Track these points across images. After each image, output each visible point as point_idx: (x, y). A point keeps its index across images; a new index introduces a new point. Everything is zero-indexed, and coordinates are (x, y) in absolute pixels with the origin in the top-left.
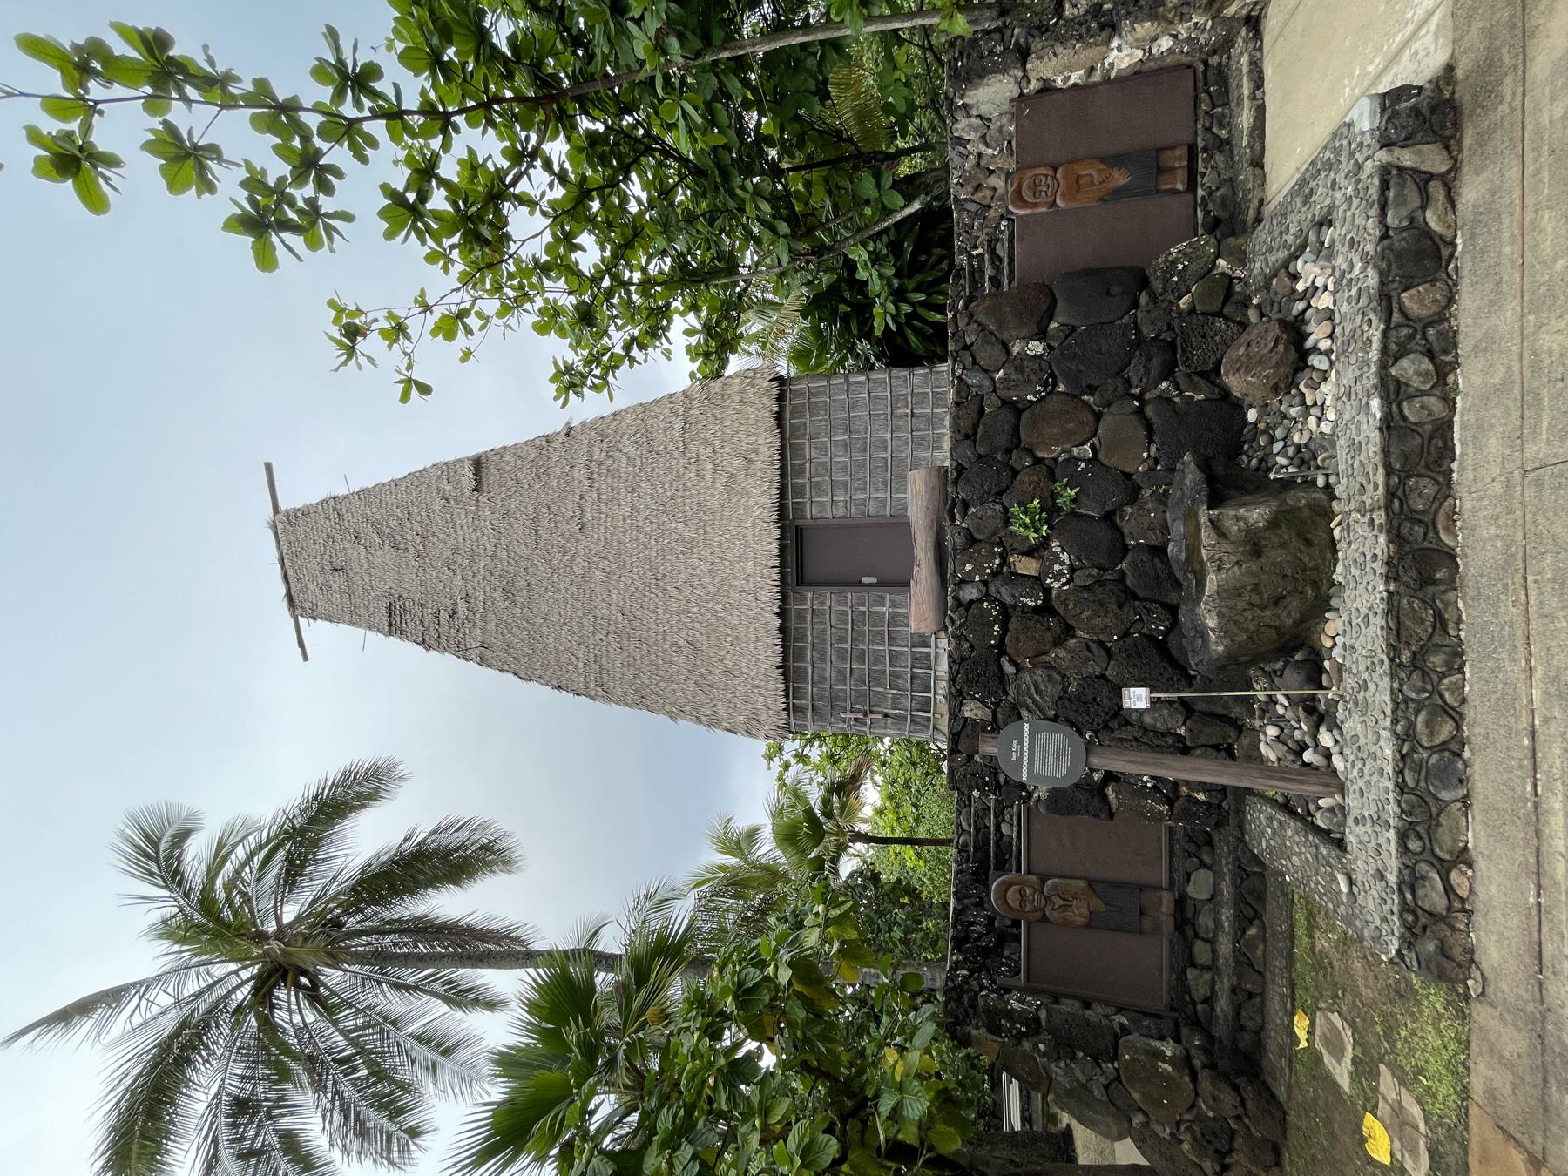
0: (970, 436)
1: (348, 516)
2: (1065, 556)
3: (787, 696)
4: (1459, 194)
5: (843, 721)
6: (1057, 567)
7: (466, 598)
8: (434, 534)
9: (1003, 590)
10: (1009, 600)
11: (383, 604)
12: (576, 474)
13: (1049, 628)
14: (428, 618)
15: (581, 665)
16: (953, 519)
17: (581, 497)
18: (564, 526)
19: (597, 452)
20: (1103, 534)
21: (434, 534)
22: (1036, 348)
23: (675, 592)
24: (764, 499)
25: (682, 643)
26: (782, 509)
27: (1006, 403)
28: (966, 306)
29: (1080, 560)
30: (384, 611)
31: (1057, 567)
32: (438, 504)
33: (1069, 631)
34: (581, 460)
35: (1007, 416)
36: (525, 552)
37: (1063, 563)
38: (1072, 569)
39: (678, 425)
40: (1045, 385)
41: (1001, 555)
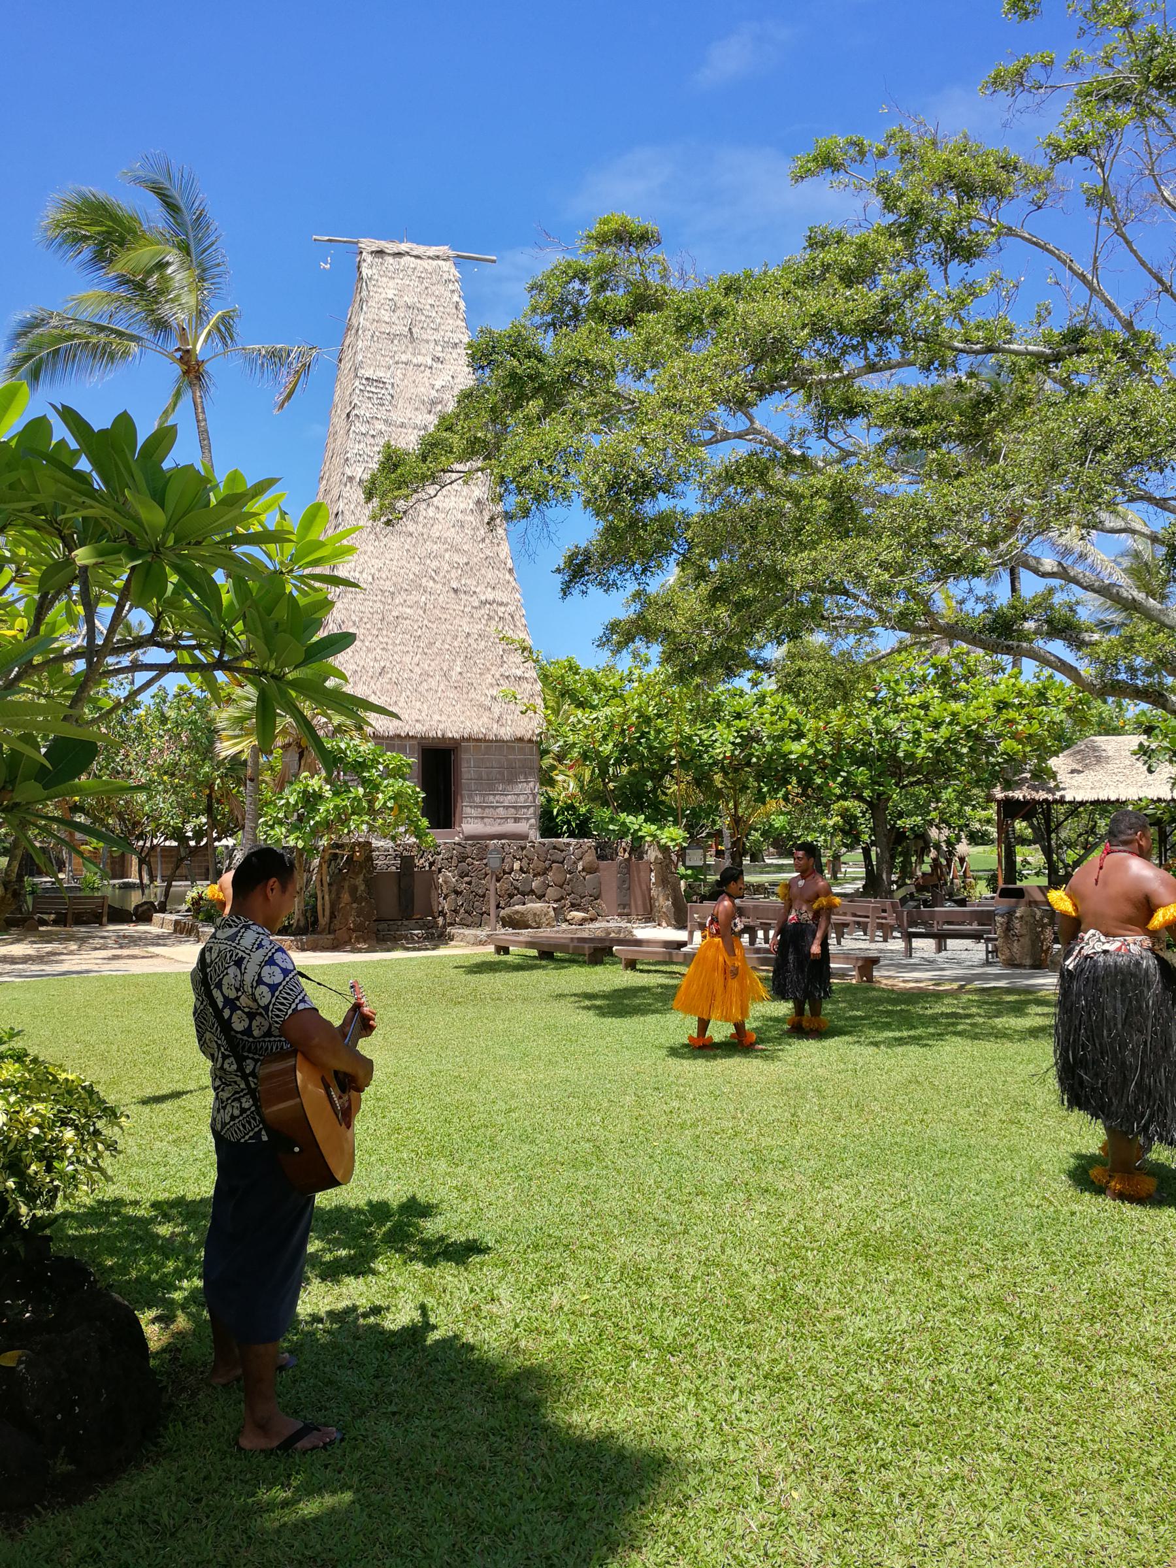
18: (454, 574)
19: (503, 609)
23: (416, 660)
24: (476, 729)
26: (469, 739)
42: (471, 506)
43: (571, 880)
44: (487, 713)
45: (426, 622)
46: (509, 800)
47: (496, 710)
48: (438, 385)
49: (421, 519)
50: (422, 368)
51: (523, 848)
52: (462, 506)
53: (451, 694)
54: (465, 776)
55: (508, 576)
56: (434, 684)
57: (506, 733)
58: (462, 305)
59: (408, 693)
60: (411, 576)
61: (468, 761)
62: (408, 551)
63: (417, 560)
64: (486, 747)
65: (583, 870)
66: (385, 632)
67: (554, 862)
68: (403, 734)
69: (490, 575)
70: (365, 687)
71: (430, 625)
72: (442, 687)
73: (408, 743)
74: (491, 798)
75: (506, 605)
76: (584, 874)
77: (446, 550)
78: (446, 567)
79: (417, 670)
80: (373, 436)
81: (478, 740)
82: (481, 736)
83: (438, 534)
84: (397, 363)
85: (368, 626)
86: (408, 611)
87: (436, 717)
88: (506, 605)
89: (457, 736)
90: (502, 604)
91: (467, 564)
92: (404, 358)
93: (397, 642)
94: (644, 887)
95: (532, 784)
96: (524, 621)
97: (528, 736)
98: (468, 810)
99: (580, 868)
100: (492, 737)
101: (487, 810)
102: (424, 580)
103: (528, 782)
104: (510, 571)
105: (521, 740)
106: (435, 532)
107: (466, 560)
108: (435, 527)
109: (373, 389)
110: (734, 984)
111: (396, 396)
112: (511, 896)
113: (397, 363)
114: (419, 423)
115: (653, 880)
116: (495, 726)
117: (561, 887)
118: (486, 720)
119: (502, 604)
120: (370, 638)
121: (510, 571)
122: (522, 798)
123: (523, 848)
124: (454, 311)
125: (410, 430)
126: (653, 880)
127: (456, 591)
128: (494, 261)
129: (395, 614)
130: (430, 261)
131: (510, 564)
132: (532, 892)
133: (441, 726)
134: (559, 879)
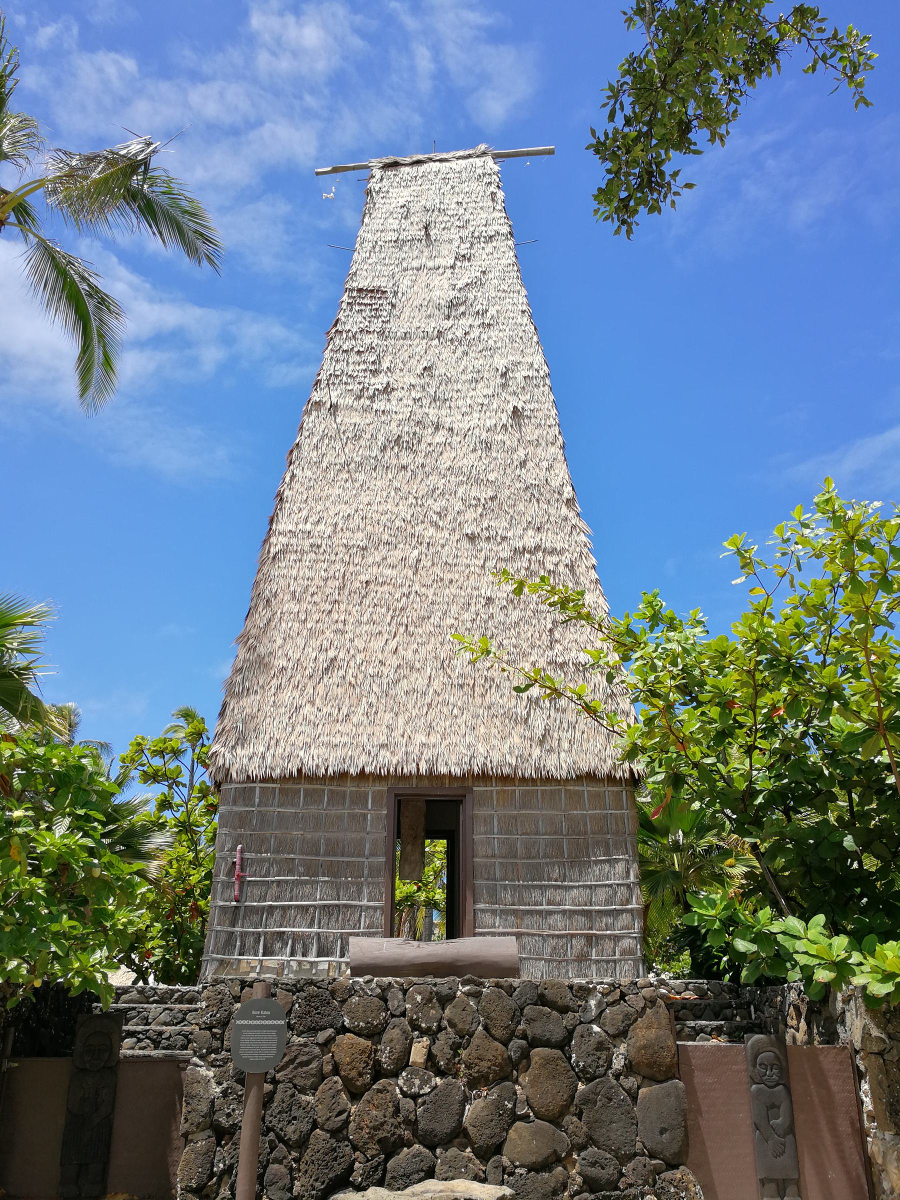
0: (542, 1000)
1: (489, 248)
2: (427, 1090)
3: (264, 780)
4: (36, 269)
5: (233, 849)
6: (417, 1082)
7: (387, 390)
8: (466, 353)
9: (397, 1031)
10: (386, 1037)
11: (382, 283)
12: (530, 532)
13: (360, 1075)
14: (368, 339)
15: (308, 527)
16: (464, 983)
17: (504, 538)
18: (470, 515)
19: (555, 559)
20: (444, 1126)
21: (466, 353)
22: (618, 1063)
23: (393, 644)
24: (496, 757)
25: (331, 654)
26: (484, 777)
27: (570, 1033)
28: (662, 997)
29: (424, 1103)
30: (376, 283)
31: (417, 1082)
32: (500, 362)
33: (355, 1096)
34: (549, 539)
35: (558, 1034)
36: (446, 461)
37: (421, 1088)
38: (415, 1097)
39: (583, 658)
40: (584, 1070)
41: (429, 1029)
42: (504, 420)
43: (587, 1100)
44: (520, 729)
45: (417, 587)
46: (571, 900)
47: (539, 722)
48: (460, 284)
49: (423, 446)
50: (441, 271)
51: (445, 1000)
52: (489, 423)
53: (456, 697)
54: (481, 850)
55: (564, 510)
56: (421, 683)
57: (559, 763)
58: (501, 195)
59: (373, 699)
60: (398, 523)
61: (488, 820)
62: (397, 489)
63: (411, 500)
64: (525, 794)
65: (630, 1068)
66: (343, 607)
67: (534, 1043)
68: (352, 771)
69: (533, 510)
70: (296, 694)
71: (424, 590)
72: (436, 685)
73: (371, 789)
74: (536, 895)
75: (561, 552)
76: (630, 1082)
77: (459, 484)
78: (458, 506)
79: (394, 661)
80: (359, 353)
81: (505, 779)
82: (506, 770)
83: (449, 463)
84: (406, 270)
85: (316, 598)
86: (388, 572)
87: (421, 738)
88: (561, 552)
89: (456, 771)
90: (553, 552)
91: (492, 499)
92: (415, 264)
93: (365, 619)
94: (844, 1127)
95: (620, 868)
96: (593, 575)
97: (605, 768)
98: (488, 919)
99: (618, 1063)
100: (530, 772)
101: (528, 920)
102: (420, 528)
103: (612, 862)
104: (569, 502)
105: (590, 777)
106: (446, 461)
107: (490, 493)
108: (445, 455)
109: (365, 301)
110: (624, 228)
111: (399, 305)
112: (390, 1148)
113: (406, 270)
114: (430, 330)
115: (868, 1104)
116: (536, 752)
117: (555, 1121)
118: (517, 740)
119: (553, 552)
120: (316, 617)
121: (569, 502)
122: (602, 895)
123: (445, 1000)
124: (490, 203)
125: (417, 341)
126: (868, 1104)
127: (472, 538)
128: (551, 152)
129: (364, 578)
130: (460, 161)
131: (568, 492)
132: (459, 1135)
133: (427, 754)
134: (551, 1094)
